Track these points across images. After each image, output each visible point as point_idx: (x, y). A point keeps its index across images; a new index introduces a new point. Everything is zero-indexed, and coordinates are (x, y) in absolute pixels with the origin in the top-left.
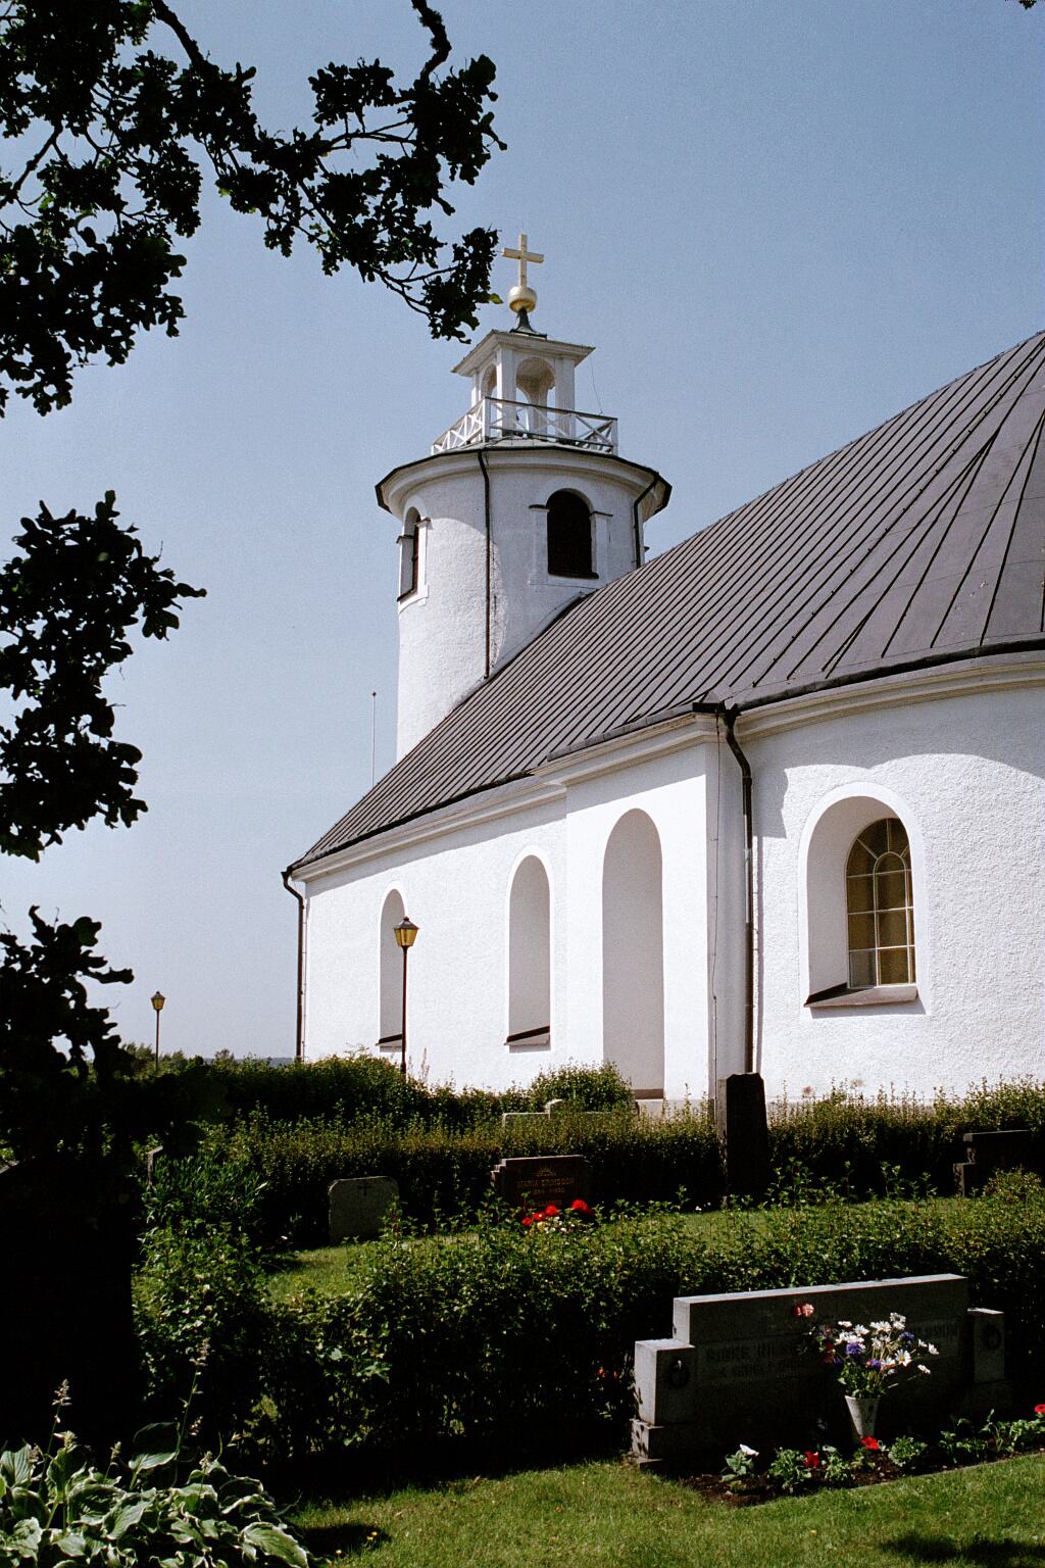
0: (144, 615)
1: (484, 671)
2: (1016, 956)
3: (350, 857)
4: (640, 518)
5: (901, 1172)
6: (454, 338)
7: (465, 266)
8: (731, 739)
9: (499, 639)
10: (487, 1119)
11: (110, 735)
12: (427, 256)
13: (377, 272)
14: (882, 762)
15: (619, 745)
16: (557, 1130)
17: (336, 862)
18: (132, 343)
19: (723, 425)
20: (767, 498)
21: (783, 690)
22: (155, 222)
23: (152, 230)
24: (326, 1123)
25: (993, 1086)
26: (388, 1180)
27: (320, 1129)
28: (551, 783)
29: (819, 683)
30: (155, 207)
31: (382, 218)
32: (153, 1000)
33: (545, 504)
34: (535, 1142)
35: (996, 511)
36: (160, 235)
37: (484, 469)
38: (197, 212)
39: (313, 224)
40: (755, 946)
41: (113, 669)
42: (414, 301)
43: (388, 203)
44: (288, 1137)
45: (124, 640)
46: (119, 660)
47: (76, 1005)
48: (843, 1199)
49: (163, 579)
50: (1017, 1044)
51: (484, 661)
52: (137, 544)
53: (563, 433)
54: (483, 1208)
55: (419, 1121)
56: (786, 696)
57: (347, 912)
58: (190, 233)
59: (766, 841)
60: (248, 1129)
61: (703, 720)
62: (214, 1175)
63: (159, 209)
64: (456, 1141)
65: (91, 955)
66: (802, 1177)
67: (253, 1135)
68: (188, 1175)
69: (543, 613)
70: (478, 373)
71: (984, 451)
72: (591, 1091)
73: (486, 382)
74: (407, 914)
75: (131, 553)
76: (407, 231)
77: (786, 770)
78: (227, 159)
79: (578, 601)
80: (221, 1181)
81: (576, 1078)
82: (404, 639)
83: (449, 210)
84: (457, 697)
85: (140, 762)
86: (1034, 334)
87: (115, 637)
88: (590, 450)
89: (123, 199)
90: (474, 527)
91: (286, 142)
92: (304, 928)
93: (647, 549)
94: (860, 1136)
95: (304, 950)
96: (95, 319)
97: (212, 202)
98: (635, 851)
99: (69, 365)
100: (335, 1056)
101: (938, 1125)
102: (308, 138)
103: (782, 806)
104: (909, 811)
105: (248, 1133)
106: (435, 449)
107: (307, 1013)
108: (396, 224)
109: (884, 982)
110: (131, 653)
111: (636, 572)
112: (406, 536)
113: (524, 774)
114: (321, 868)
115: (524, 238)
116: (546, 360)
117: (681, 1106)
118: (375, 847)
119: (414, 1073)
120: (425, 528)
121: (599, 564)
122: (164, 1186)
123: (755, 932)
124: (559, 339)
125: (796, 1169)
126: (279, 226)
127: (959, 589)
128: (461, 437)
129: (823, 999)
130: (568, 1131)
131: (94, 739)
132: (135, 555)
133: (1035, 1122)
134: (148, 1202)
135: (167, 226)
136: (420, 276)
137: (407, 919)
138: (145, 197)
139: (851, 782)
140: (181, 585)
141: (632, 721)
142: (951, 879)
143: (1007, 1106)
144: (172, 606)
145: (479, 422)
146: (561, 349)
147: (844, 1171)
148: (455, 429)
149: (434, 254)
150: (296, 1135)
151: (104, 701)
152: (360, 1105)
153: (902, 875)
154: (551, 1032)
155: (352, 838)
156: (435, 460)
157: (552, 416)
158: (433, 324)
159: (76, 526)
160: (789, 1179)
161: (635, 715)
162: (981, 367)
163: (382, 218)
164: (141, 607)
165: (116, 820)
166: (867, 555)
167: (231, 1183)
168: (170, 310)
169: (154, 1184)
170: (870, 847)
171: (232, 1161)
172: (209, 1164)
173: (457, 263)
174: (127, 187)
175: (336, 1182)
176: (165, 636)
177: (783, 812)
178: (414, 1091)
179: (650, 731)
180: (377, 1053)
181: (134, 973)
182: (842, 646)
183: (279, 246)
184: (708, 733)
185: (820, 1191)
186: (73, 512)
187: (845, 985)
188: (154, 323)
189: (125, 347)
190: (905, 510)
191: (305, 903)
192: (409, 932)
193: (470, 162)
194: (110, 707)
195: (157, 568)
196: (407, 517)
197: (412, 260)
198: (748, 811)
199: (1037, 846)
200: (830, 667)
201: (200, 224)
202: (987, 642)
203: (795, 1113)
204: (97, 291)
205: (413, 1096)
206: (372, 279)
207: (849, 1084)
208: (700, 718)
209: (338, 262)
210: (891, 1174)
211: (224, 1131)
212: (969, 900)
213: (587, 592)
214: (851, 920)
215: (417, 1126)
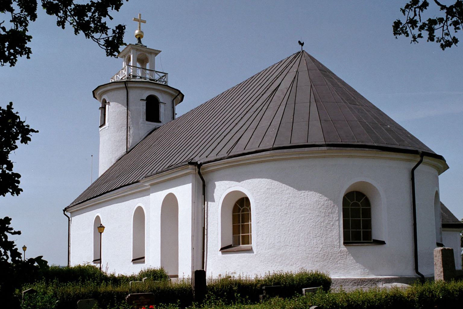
2: (280, 237)
5: (240, 296)
6: (113, 56)
7: (116, 35)
8: (199, 173)
9: (130, 140)
10: (125, 283)
11: (12, 170)
12: (105, 32)
13: (90, 36)
14: (243, 181)
15: (165, 175)
16: (145, 286)
17: (80, 207)
20: (212, 100)
21: (215, 158)
22: (23, 16)
23: (23, 19)
24: (76, 283)
25: (272, 273)
26: (95, 300)
27: (74, 285)
28: (146, 184)
29: (225, 157)
30: (23, 12)
31: (92, 20)
32: (23, 248)
33: (145, 99)
37: (126, 88)
38: (36, 14)
39: (71, 19)
40: (206, 234)
41: (12, 152)
42: (101, 45)
43: (93, 15)
44: (65, 288)
45: (16, 144)
46: (14, 150)
47: (5, 240)
48: (224, 303)
49: (26, 127)
50: (280, 262)
51: (126, 147)
52: (19, 117)
53: (151, 77)
54: (121, 306)
55: (104, 283)
57: (83, 223)
59: (209, 203)
60: (53, 285)
61: (191, 167)
63: (24, 12)
64: (115, 289)
65: (9, 227)
66: (213, 297)
67: (54, 287)
68: (35, 298)
69: (144, 133)
70: (125, 57)
72: (156, 275)
74: (102, 223)
75: (17, 120)
76: (99, 24)
79: (155, 129)
80: (45, 300)
82: (101, 140)
83: (111, 18)
84: (117, 158)
85: (21, 178)
86: (292, 54)
87: (13, 143)
88: (159, 83)
89: (13, 8)
90: (123, 105)
93: (176, 114)
95: (70, 233)
98: (170, 206)
100: (79, 265)
103: (214, 193)
105: (53, 286)
106: (111, 80)
107: (71, 252)
108: (96, 22)
109: (243, 244)
112: (102, 107)
115: (140, 15)
116: (146, 54)
118: (92, 203)
119: (104, 270)
120: (108, 105)
121: (162, 118)
122: (27, 302)
124: (150, 48)
125: (211, 295)
126: (61, 20)
128: (120, 77)
129: (225, 249)
131: (7, 171)
132: (18, 120)
133: (283, 283)
134: (22, 306)
135: (27, 18)
137: (101, 224)
138: (20, 8)
139: (235, 186)
140: (31, 129)
142: (262, 215)
144: (29, 135)
146: (152, 51)
148: (118, 74)
149: (107, 31)
150: (67, 287)
151: (10, 161)
153: (249, 214)
154: (145, 258)
155: (85, 200)
156: (111, 84)
157: (148, 72)
158: (107, 52)
161: (171, 165)
162: (277, 63)
163: (92, 20)
165: (14, 194)
167: (48, 301)
169: (24, 301)
170: (240, 206)
173: (113, 35)
175: (79, 301)
176: (27, 143)
178: (103, 275)
179: (175, 170)
180: (92, 264)
181: (21, 232)
182: (233, 146)
183: (61, 26)
187: (231, 245)
188: (23, 55)
189: (14, 61)
191: (70, 219)
192: (102, 228)
194: (12, 163)
195: (24, 124)
196: (102, 101)
197: (100, 33)
198: (204, 194)
199: (287, 206)
200: (229, 152)
201: (37, 17)
202: (275, 146)
203: (214, 281)
205: (103, 276)
206: (89, 38)
207: (231, 273)
208: (190, 166)
211: (45, 286)
212: (267, 221)
214: (233, 226)
215: (103, 284)
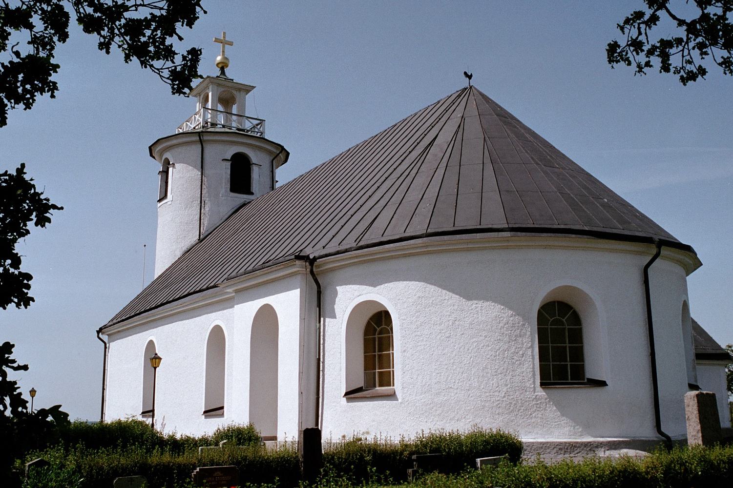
0: (35, 217)
1: (198, 237)
3: (130, 324)
4: (274, 169)
5: (376, 470)
6: (181, 95)
7: (187, 63)
8: (312, 272)
11: (19, 269)
12: (170, 58)
13: (148, 65)
15: (259, 275)
16: (224, 454)
18: (35, 100)
19: (313, 128)
20: (333, 161)
23: (47, 39)
24: (113, 450)
28: (228, 291)
29: (353, 247)
31: (151, 41)
32: (30, 392)
33: (229, 159)
34: (213, 460)
35: (435, 172)
36: (50, 42)
37: (201, 142)
38: (68, 32)
39: (120, 40)
40: (321, 369)
41: (21, 240)
42: (164, 77)
44: (95, 457)
45: (27, 228)
49: (44, 202)
51: (198, 232)
52: (34, 186)
55: (158, 449)
56: (338, 253)
57: (127, 351)
58: (64, 41)
59: (327, 320)
60: (75, 453)
61: (299, 263)
62: (58, 475)
63: (50, 30)
65: (9, 358)
66: (332, 473)
69: (226, 210)
70: (200, 96)
71: (431, 144)
73: (204, 100)
75: (31, 190)
76: (162, 47)
77: (337, 287)
78: (82, 10)
81: (235, 430)
83: (181, 39)
84: (185, 249)
86: (455, 92)
88: (252, 134)
91: (109, 5)
92: (107, 358)
93: (277, 181)
94: (365, 457)
96: (18, 89)
97: (74, 28)
98: (265, 325)
99: (6, 109)
100: (119, 419)
101: (401, 452)
102: (119, 4)
103: (335, 304)
104: (393, 307)
106: (178, 131)
107: (107, 399)
108: (157, 44)
109: (380, 386)
110: (29, 233)
111: (271, 192)
112: (163, 171)
113: (215, 286)
114: (117, 328)
115: (224, 33)
117: (282, 443)
119: (158, 427)
121: (255, 187)
123: (321, 362)
127: (418, 206)
128: (191, 125)
129: (352, 394)
130: (229, 455)
131: (12, 270)
132: (32, 191)
133: (445, 450)
136: (167, 67)
137: (156, 354)
138: (44, 24)
141: (267, 262)
143: (432, 442)
144: (48, 214)
145: (199, 119)
146: (241, 87)
147: (351, 470)
149: (174, 58)
150: (99, 456)
151: (17, 254)
152: (130, 442)
157: (234, 117)
159: (7, 177)
160: (326, 474)
163: (151, 41)
164: (34, 213)
165: (21, 305)
166: (377, 189)
167: (66, 479)
168: (52, 87)
171: (67, 468)
172: (55, 470)
173: (183, 63)
174: (36, 20)
175: (117, 479)
177: (335, 307)
179: (274, 268)
180: (140, 418)
181: (29, 366)
182: (364, 231)
184: (301, 269)
185: (341, 479)
186: (6, 171)
187: (362, 387)
188: (45, 92)
190: (395, 169)
191: (107, 345)
192: (157, 360)
193: (191, 21)
195: (42, 197)
196: (164, 162)
197: (164, 60)
198: (319, 305)
203: (335, 446)
204: (20, 77)
208: (298, 262)
209: (131, 58)
210: (372, 472)
211: (63, 454)
213: (248, 201)
214: (365, 357)
